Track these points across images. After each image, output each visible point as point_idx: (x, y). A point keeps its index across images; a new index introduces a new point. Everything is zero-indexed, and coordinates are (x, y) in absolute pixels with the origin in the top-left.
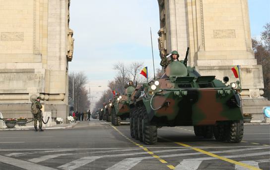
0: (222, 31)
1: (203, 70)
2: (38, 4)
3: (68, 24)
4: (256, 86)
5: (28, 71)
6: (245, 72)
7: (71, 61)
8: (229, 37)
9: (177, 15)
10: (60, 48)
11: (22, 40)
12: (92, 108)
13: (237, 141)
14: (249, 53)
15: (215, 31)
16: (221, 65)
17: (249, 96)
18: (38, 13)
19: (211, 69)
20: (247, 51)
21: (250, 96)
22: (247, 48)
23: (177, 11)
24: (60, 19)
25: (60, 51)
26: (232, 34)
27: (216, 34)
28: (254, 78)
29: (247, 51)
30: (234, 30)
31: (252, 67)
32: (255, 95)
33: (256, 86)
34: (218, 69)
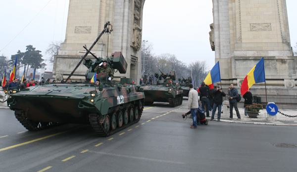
0: (259, 24)
1: (239, 60)
2: (104, 4)
3: (137, 20)
4: (291, 77)
5: (63, 56)
6: (280, 63)
7: (32, 46)
8: (265, 30)
9: (220, 11)
10: (122, 40)
11: (90, 33)
12: (174, 97)
13: (207, 125)
14: (284, 44)
15: (252, 25)
16: (256, 55)
17: (284, 85)
18: (104, 11)
19: (247, 60)
20: (283, 43)
21: (238, 85)
22: (283, 40)
23: (220, 8)
24: (124, 16)
25: (122, 42)
26: (268, 27)
27: (253, 27)
28: (289, 68)
29: (283, 43)
30: (270, 24)
31: (287, 58)
32: (290, 85)
33: (291, 77)
34: (253, 60)
